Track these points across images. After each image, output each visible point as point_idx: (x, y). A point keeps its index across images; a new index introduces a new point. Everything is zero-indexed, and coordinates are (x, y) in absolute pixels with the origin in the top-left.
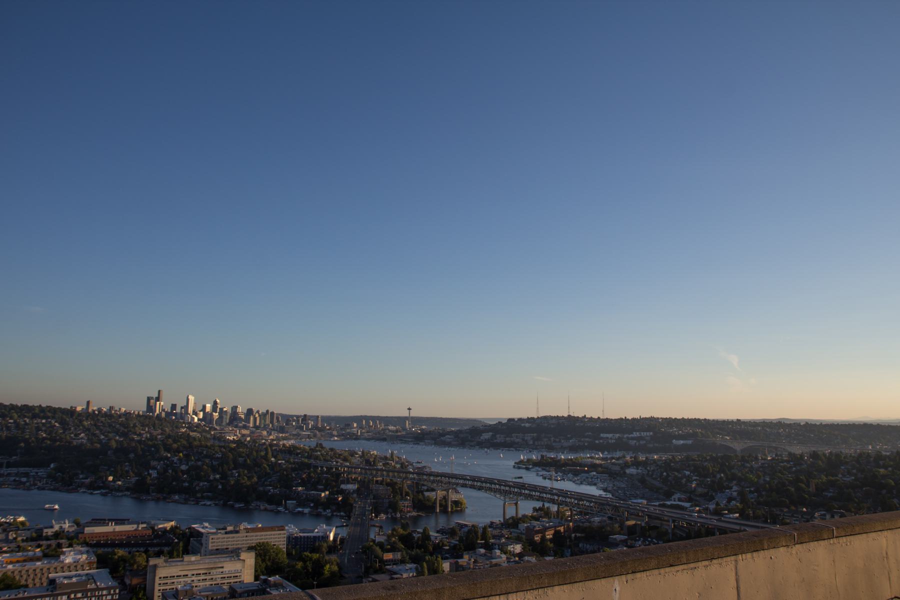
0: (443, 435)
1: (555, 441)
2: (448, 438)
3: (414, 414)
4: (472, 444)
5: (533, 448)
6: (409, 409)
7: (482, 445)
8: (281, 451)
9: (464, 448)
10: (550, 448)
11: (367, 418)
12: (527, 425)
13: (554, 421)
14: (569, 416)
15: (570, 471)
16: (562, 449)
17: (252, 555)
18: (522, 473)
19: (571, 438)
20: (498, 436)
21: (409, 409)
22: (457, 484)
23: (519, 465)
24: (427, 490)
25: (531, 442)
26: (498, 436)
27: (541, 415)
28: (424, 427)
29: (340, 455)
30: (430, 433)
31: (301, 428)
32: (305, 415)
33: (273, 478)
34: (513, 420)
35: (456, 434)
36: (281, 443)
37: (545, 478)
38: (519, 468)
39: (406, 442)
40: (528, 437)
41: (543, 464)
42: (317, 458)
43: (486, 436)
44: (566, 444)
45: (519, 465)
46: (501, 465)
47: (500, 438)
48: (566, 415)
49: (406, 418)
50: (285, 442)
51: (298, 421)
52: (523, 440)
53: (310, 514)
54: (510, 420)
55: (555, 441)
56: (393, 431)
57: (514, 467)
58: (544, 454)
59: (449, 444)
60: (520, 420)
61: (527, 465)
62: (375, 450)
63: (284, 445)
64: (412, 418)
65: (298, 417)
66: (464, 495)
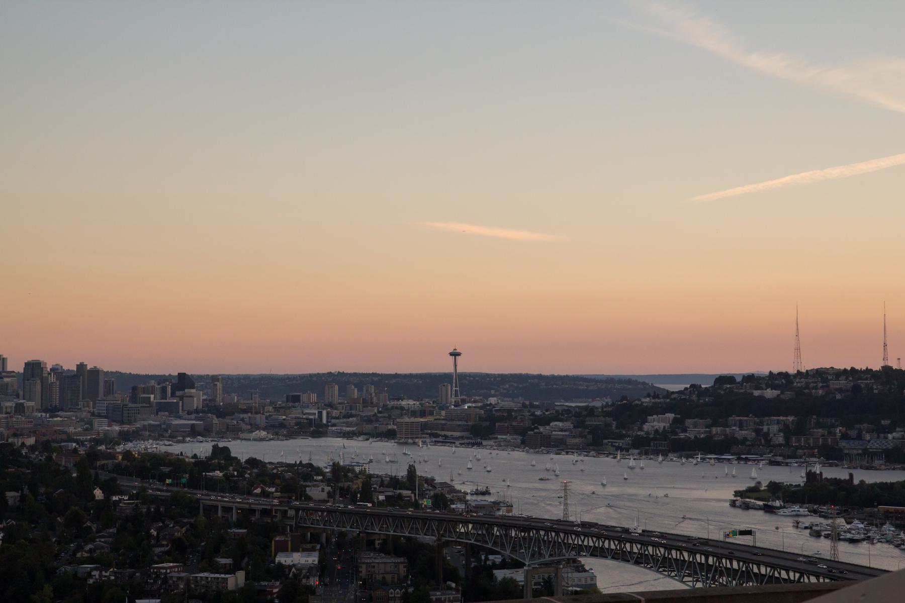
0: (545, 421)
1: (845, 437)
2: (557, 428)
3: (466, 366)
4: (620, 443)
5: (782, 455)
6: (455, 354)
7: (647, 446)
8: (119, 470)
9: (599, 453)
10: (832, 455)
11: (341, 380)
12: (770, 393)
13: (842, 382)
14: (887, 369)
15: (887, 517)
16: (868, 459)
17: (847, 477)
18: (754, 520)
19: (891, 429)
20: (689, 422)
21: (455, 354)
22: (580, 549)
23: (745, 499)
24: (503, 565)
25: (780, 439)
26: (689, 422)
27: (809, 364)
28: (493, 400)
29: (274, 477)
30: (508, 415)
31: (171, 409)
32: (182, 376)
33: (98, 542)
34: (730, 379)
35: (579, 417)
36: (120, 449)
37: (817, 535)
38: (747, 507)
39: (446, 441)
40: (773, 428)
41: (815, 495)
42: (212, 486)
43: (657, 423)
44: (875, 444)
45: (745, 499)
46: (699, 498)
47: (695, 430)
48: (876, 366)
49: (445, 378)
50: (129, 446)
51: (164, 390)
52: (758, 432)
53: (491, 525)
54: (722, 380)
55: (845, 437)
56: (414, 413)
57: (733, 504)
58: (817, 469)
59: (560, 446)
60: (750, 378)
61: (773, 498)
62: (380, 457)
63: (127, 455)
64: (462, 377)
65: (161, 379)
66: (807, 513)
